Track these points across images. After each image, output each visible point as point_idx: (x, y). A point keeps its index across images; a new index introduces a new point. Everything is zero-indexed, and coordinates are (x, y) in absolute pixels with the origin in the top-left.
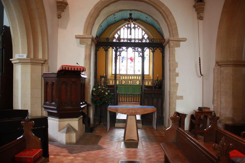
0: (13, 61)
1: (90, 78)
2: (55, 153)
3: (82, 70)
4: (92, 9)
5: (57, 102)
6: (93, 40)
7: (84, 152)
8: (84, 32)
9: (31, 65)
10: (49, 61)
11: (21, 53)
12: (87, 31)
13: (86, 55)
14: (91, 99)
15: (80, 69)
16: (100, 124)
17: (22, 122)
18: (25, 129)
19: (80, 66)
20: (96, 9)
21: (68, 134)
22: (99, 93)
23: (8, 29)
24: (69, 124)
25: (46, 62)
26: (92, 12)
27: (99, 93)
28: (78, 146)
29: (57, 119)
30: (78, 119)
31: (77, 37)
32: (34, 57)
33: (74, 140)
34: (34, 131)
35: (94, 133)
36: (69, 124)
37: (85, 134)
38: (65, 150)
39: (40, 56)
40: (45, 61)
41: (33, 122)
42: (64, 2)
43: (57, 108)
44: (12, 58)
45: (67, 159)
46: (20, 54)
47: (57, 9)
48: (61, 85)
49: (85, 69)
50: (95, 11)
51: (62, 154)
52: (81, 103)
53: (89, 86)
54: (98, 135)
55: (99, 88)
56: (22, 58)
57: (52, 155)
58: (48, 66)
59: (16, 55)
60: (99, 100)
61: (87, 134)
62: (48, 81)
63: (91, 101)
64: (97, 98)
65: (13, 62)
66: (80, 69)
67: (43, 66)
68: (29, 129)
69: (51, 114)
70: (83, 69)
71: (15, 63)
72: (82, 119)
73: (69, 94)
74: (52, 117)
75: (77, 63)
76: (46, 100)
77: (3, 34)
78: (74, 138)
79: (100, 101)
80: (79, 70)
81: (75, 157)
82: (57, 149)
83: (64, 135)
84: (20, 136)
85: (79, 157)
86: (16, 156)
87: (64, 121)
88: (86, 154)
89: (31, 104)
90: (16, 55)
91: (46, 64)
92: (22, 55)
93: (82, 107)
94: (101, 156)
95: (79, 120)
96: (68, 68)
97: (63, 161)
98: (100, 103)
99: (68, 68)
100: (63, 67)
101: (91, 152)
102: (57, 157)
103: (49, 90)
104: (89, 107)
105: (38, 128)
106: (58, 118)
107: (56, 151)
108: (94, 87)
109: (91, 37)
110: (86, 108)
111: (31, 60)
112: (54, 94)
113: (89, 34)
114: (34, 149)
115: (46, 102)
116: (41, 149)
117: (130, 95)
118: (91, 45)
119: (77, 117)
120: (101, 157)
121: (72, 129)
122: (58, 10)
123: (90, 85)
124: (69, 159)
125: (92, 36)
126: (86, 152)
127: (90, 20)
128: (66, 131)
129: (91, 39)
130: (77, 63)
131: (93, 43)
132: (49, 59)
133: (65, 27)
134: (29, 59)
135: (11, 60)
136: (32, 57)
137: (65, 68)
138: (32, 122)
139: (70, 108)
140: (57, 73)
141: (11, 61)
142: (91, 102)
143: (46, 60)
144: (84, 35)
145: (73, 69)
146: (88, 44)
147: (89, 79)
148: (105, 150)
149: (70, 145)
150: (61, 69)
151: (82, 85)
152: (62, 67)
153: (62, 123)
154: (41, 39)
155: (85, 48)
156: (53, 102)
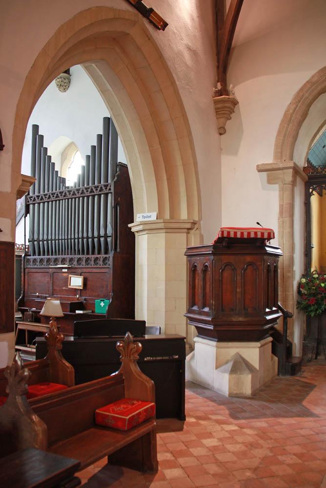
0: (134, 227)
2: (199, 414)
3: (266, 236)
4: (290, 103)
5: (213, 307)
6: (296, 170)
8: (276, 157)
9: (166, 233)
10: (202, 222)
11: (147, 211)
12: (281, 153)
13: (281, 206)
14: (295, 303)
15: (262, 234)
16: (316, 358)
17: (118, 344)
18: (123, 358)
19: (264, 227)
20: (299, 101)
21: (234, 376)
22: (314, 288)
23: (124, 167)
24: (238, 354)
25: (196, 226)
26: (291, 111)
27: (314, 288)
28: (256, 403)
29: (214, 343)
30: (258, 344)
31: (260, 170)
32: (172, 217)
33: (247, 389)
34: (141, 363)
35: (297, 378)
36: (238, 354)
37: (277, 377)
38: (225, 408)
39: (184, 215)
40: (194, 223)
41: (138, 346)
42: (229, 98)
43: (212, 319)
44: (133, 222)
45: (223, 429)
46: (145, 212)
47: (216, 116)
48: (222, 271)
49: (274, 234)
50: (297, 105)
51: (214, 417)
52: (267, 310)
54: (306, 383)
55: (314, 278)
57: (191, 416)
59: (138, 215)
60: (314, 305)
61: (283, 377)
62: (196, 264)
64: (309, 300)
65: (133, 230)
66: (262, 234)
67: (189, 235)
68: (132, 358)
69: (202, 332)
71: (137, 232)
72: (270, 345)
73: (238, 290)
75: (258, 223)
76: (192, 301)
77: (116, 178)
78: (247, 384)
79: (316, 306)
80: (259, 236)
81: (240, 427)
82: (209, 406)
83: (226, 377)
84: (115, 372)
85: (251, 428)
86: (97, 411)
87: (228, 347)
88: (268, 423)
90: (138, 215)
91: (195, 229)
92: (149, 214)
93: (269, 318)
94: (302, 432)
95: (261, 346)
96: (235, 233)
97: (213, 433)
98: (317, 310)
99: (235, 233)
100: (223, 232)
101: (281, 420)
102: (202, 422)
103: (199, 282)
104: (288, 318)
105: (164, 358)
106: (217, 340)
108: (303, 275)
109: (293, 165)
111: (164, 222)
112: (208, 290)
113: (286, 161)
114: (138, 400)
115: (193, 306)
116: (153, 404)
117: (37, 201)
118: (294, 183)
119: (257, 340)
120: (303, 436)
122: (217, 118)
123: (293, 272)
124: (227, 431)
125: (295, 163)
127: (287, 128)
128: (230, 369)
129: (291, 171)
130: (258, 223)
131: (298, 179)
133: (235, 152)
134: (162, 221)
135: (129, 225)
136: (167, 216)
137: (229, 233)
138: (138, 346)
139: (241, 319)
141: (130, 228)
142: (297, 308)
144: (275, 162)
145: (245, 236)
146: (284, 181)
147: (292, 259)
148: (317, 419)
151: (268, 271)
152: (221, 232)
153: (223, 350)
154: (184, 180)
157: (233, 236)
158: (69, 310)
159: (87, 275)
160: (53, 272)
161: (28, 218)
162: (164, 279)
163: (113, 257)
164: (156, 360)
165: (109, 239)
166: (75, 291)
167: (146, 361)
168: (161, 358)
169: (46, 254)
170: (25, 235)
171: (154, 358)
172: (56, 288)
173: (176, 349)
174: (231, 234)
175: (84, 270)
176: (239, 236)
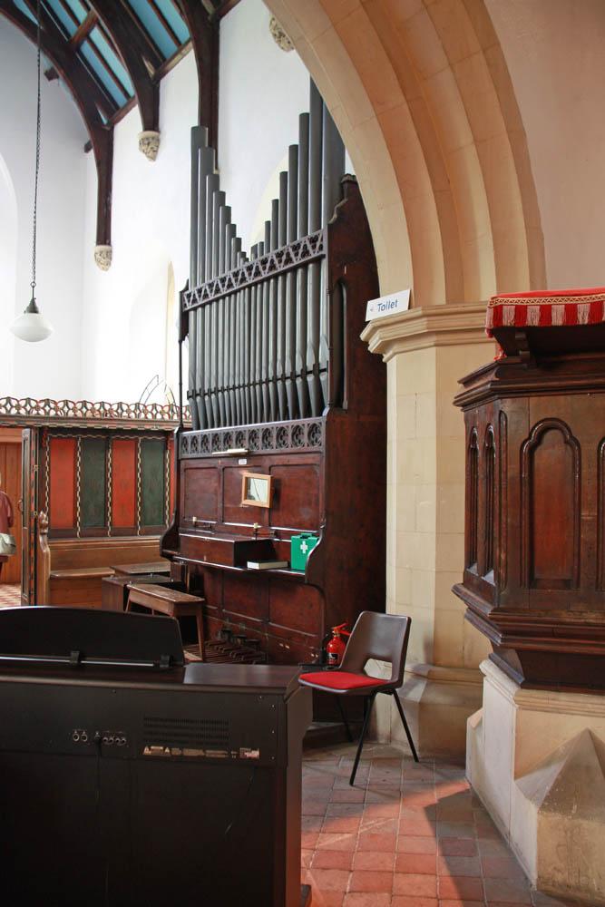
9: (436, 345)
21: (556, 817)
56: (391, 316)
87: (558, 711)
105: (210, 753)
136: (439, 297)
145: (558, 319)
153: (540, 718)
157: (536, 323)
158: (232, 559)
159: (280, 472)
160: (223, 466)
161: (186, 343)
162: (434, 481)
163: (326, 423)
164: (182, 756)
165: (324, 377)
166: (256, 512)
167: (147, 756)
168: (201, 753)
169: (228, 424)
170: (181, 384)
171: (176, 751)
172: (228, 505)
173: (181, 749)
174: (554, 314)
175: (277, 460)
176: (558, 319)
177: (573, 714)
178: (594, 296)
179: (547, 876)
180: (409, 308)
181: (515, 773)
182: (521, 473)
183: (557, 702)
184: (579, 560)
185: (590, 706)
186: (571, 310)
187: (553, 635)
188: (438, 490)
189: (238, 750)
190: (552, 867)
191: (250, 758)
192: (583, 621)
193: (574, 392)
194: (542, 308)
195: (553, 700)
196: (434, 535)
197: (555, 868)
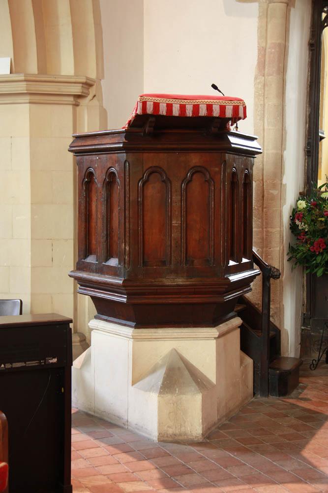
1: (282, 156)
3: (229, 113)
7: (229, 485)
9: (30, 103)
13: (262, 52)
21: (168, 397)
22: (323, 219)
25: (92, 91)
27: (323, 219)
28: (211, 454)
29: (128, 331)
30: (214, 332)
38: (153, 467)
39: (67, 66)
40: (88, 85)
49: (245, 108)
53: (275, 192)
54: (309, 411)
58: (101, 106)
61: (264, 399)
63: (286, 258)
64: (312, 244)
67: (78, 108)
69: (105, 309)
70: (236, 109)
72: (236, 336)
74: (110, 318)
75: (214, 87)
76: (85, 246)
80: (216, 113)
83: (154, 398)
87: (156, 339)
89: (33, 267)
91: (90, 97)
93: (234, 278)
95: (221, 336)
100: (144, 104)
103: (98, 208)
104: (272, 280)
105: (30, 364)
106: (134, 324)
107: (108, 470)
110: (256, 286)
111: (26, 81)
112: (115, 223)
115: (86, 256)
119: (213, 322)
121: (186, 372)
123: (281, 187)
126: (241, 487)
128: (160, 383)
130: (214, 87)
132: (103, 77)
136: (33, 67)
137: (156, 106)
139: (180, 281)
140: (126, 131)
143: (91, 82)
145: (189, 113)
149: (175, 447)
150: (139, 112)
151: (233, 184)
152: (140, 105)
153: (147, 345)
155: (260, 17)
156: (112, 257)
168: (23, 364)
171: (8, 366)
173: (11, 364)
177: (165, 341)
178: (194, 101)
179: (163, 433)
180: (11, 73)
181: (133, 382)
182: (138, 199)
183: (157, 334)
184: (171, 249)
185: (175, 334)
186: (183, 108)
187: (157, 294)
188: (32, 208)
189: (45, 360)
190: (167, 426)
191: (52, 363)
192: (176, 283)
193: (196, 151)
194: (168, 105)
195: (155, 333)
196: (30, 240)
197: (168, 427)
